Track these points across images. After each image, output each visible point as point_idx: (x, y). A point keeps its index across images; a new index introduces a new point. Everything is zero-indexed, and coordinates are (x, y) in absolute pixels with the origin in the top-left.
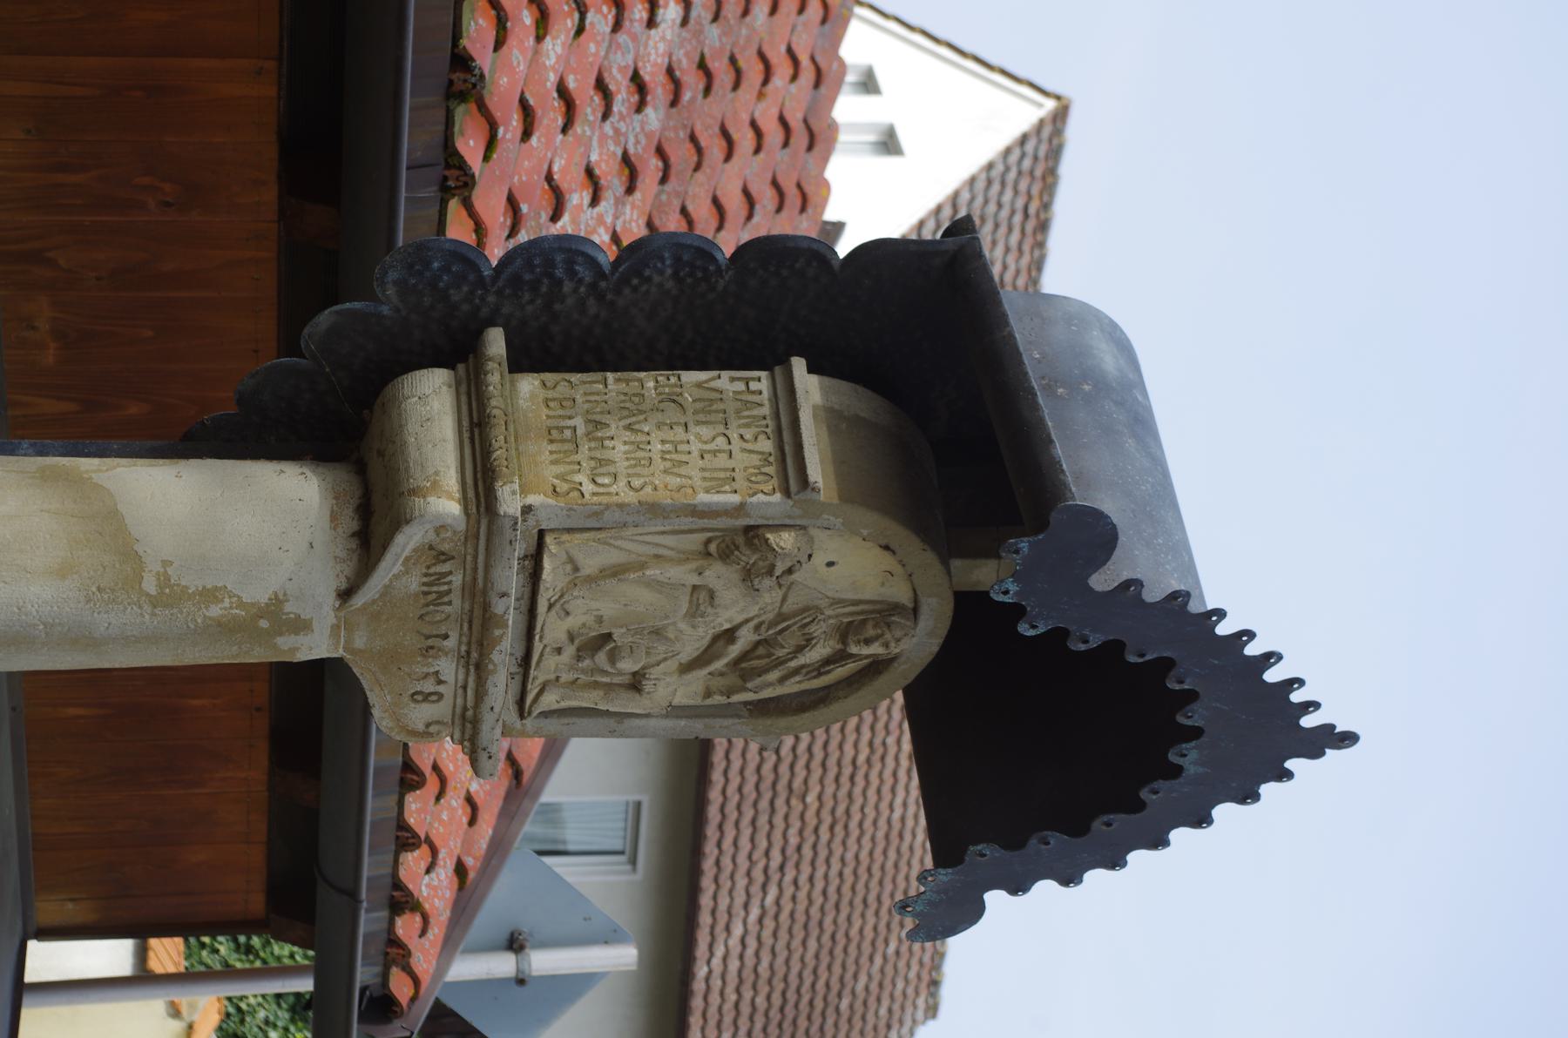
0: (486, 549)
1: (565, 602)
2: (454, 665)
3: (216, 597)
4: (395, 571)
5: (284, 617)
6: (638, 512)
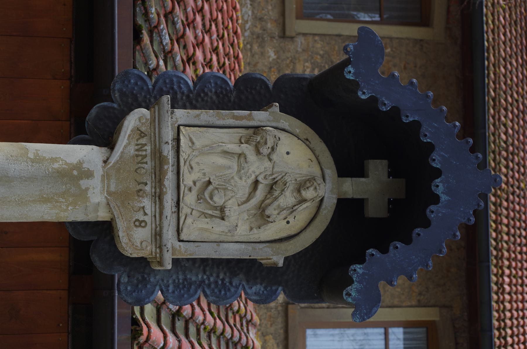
0: (159, 124)
1: (190, 160)
2: (150, 203)
3: (56, 160)
4: (124, 144)
5: (83, 169)
6: (213, 115)
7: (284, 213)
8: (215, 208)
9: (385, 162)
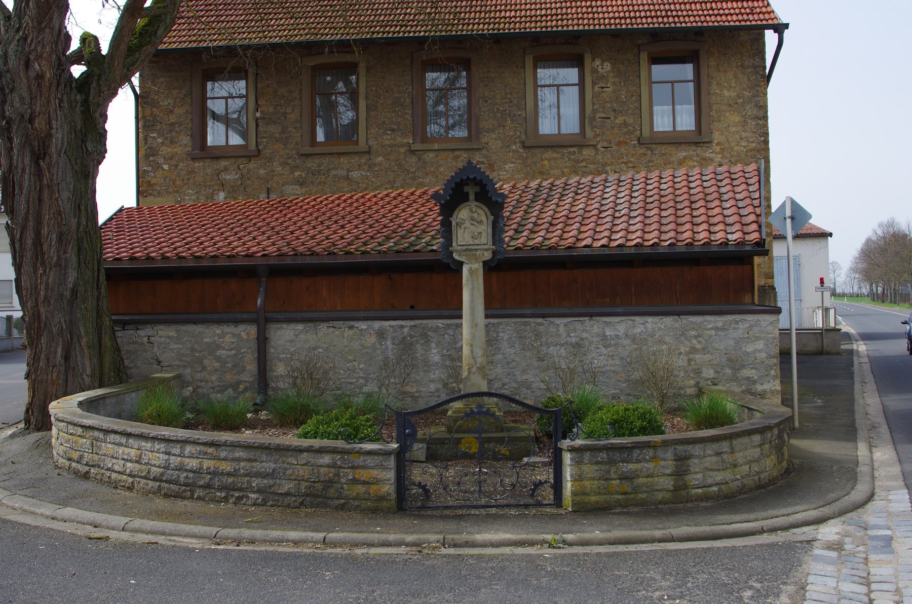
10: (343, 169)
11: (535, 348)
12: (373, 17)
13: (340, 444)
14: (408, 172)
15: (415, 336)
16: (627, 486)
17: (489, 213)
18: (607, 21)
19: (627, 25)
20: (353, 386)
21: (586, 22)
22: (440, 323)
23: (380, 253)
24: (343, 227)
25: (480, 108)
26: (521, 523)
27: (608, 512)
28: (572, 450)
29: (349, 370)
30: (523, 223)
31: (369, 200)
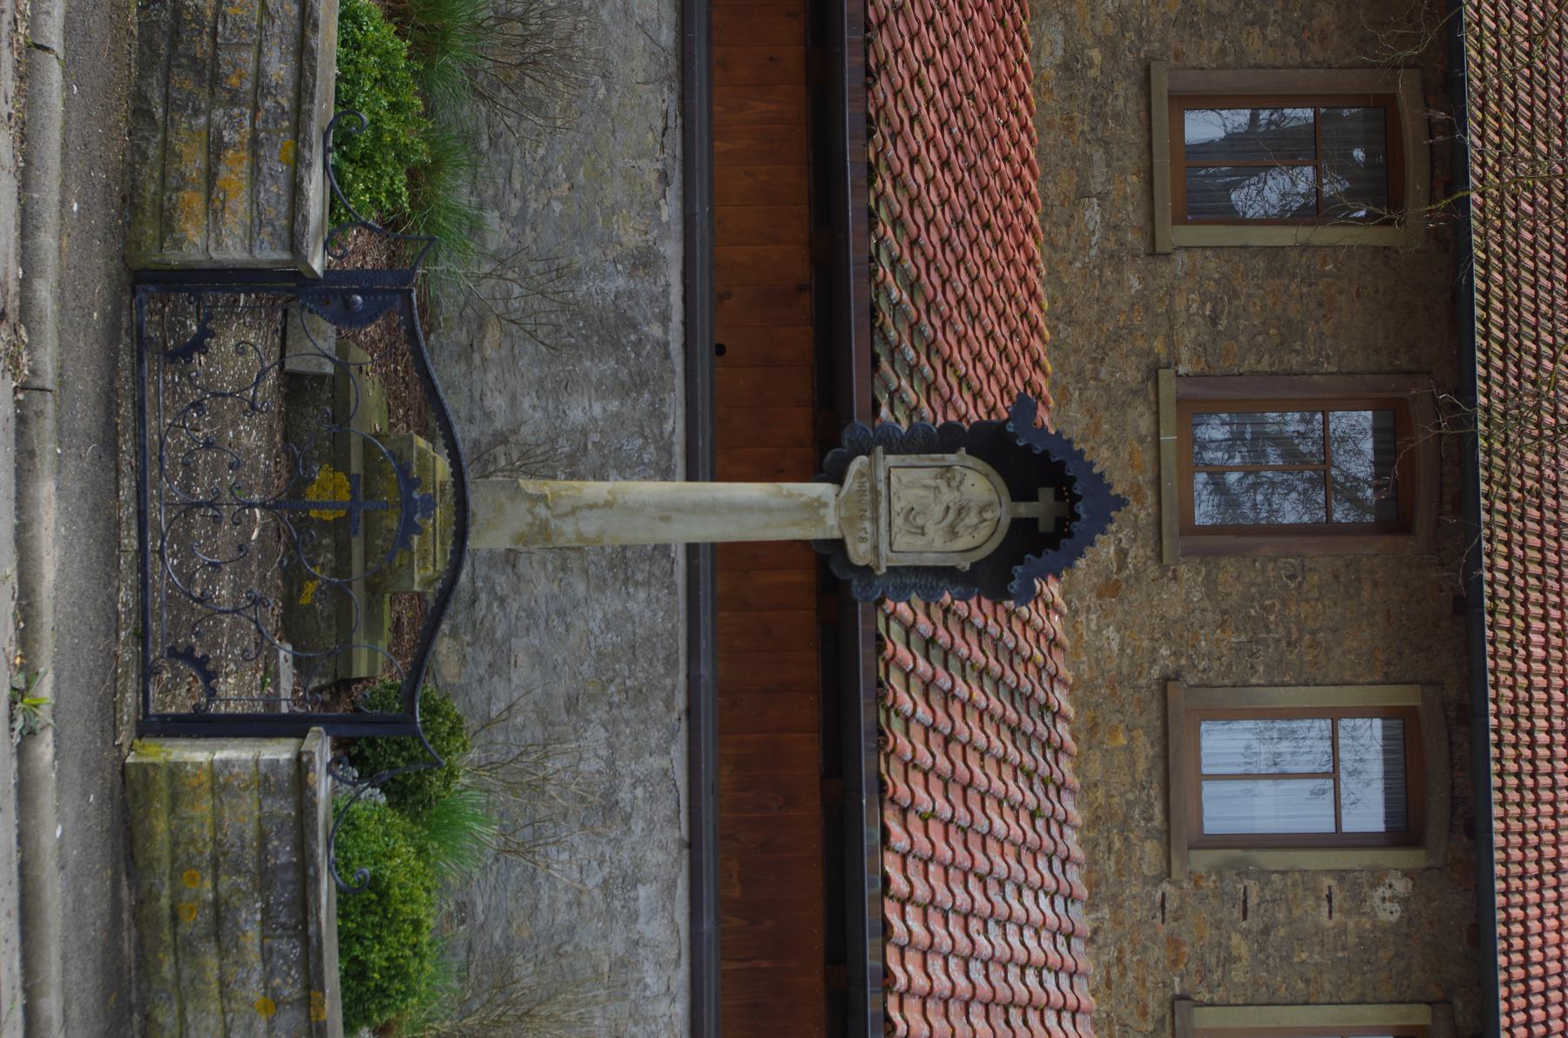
7: (970, 530)
8: (918, 527)
9: (1052, 489)
10: (1109, 181)
11: (604, 688)
12: (1530, 264)
13: (323, 108)
14: (1098, 361)
15: (638, 355)
16: (195, 921)
17: (978, 556)
18: (1516, 913)
19: (1506, 969)
20: (500, 181)
21: (1516, 854)
22: (675, 423)
23: (871, 259)
24: (945, 164)
25: (1275, 560)
26: (90, 614)
27: (122, 865)
28: (301, 766)
29: (546, 172)
30: (953, 663)
31: (1021, 245)
